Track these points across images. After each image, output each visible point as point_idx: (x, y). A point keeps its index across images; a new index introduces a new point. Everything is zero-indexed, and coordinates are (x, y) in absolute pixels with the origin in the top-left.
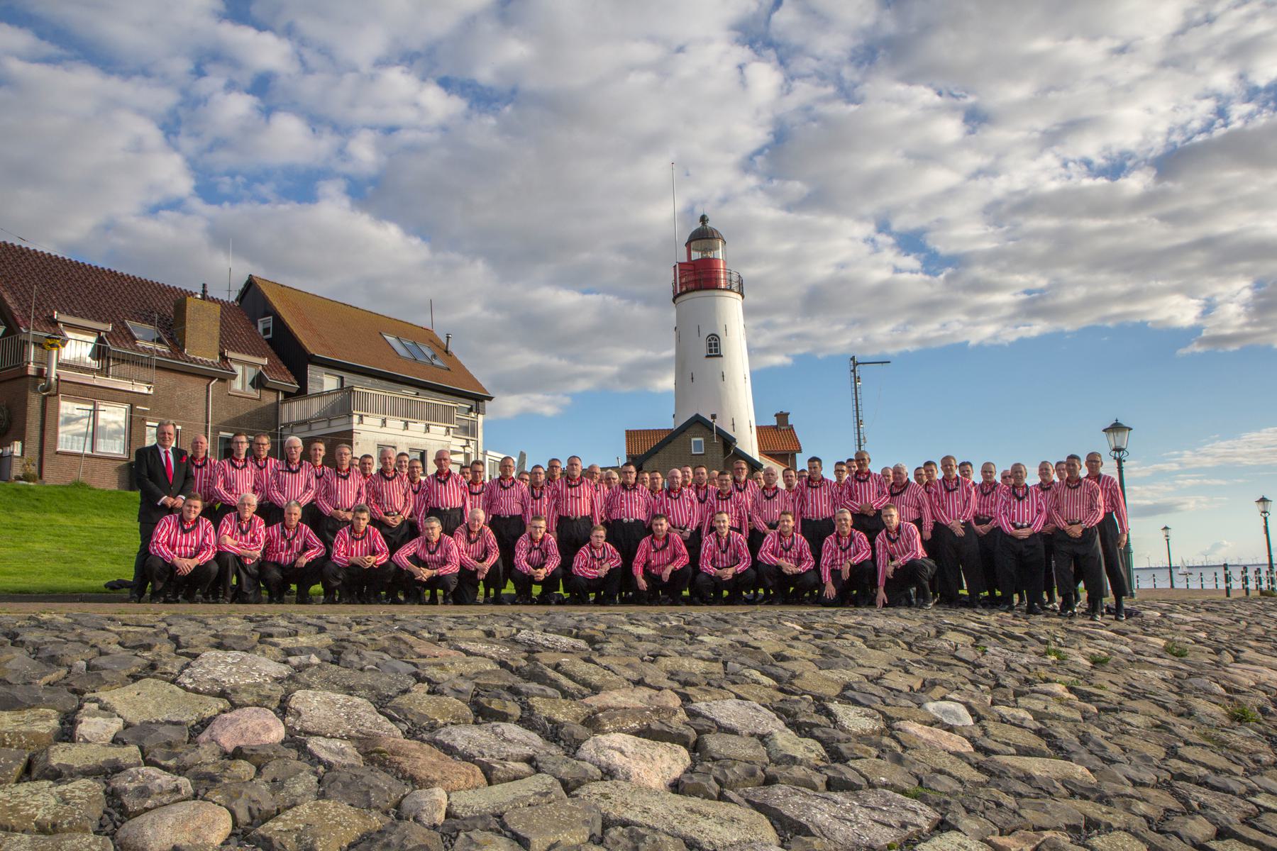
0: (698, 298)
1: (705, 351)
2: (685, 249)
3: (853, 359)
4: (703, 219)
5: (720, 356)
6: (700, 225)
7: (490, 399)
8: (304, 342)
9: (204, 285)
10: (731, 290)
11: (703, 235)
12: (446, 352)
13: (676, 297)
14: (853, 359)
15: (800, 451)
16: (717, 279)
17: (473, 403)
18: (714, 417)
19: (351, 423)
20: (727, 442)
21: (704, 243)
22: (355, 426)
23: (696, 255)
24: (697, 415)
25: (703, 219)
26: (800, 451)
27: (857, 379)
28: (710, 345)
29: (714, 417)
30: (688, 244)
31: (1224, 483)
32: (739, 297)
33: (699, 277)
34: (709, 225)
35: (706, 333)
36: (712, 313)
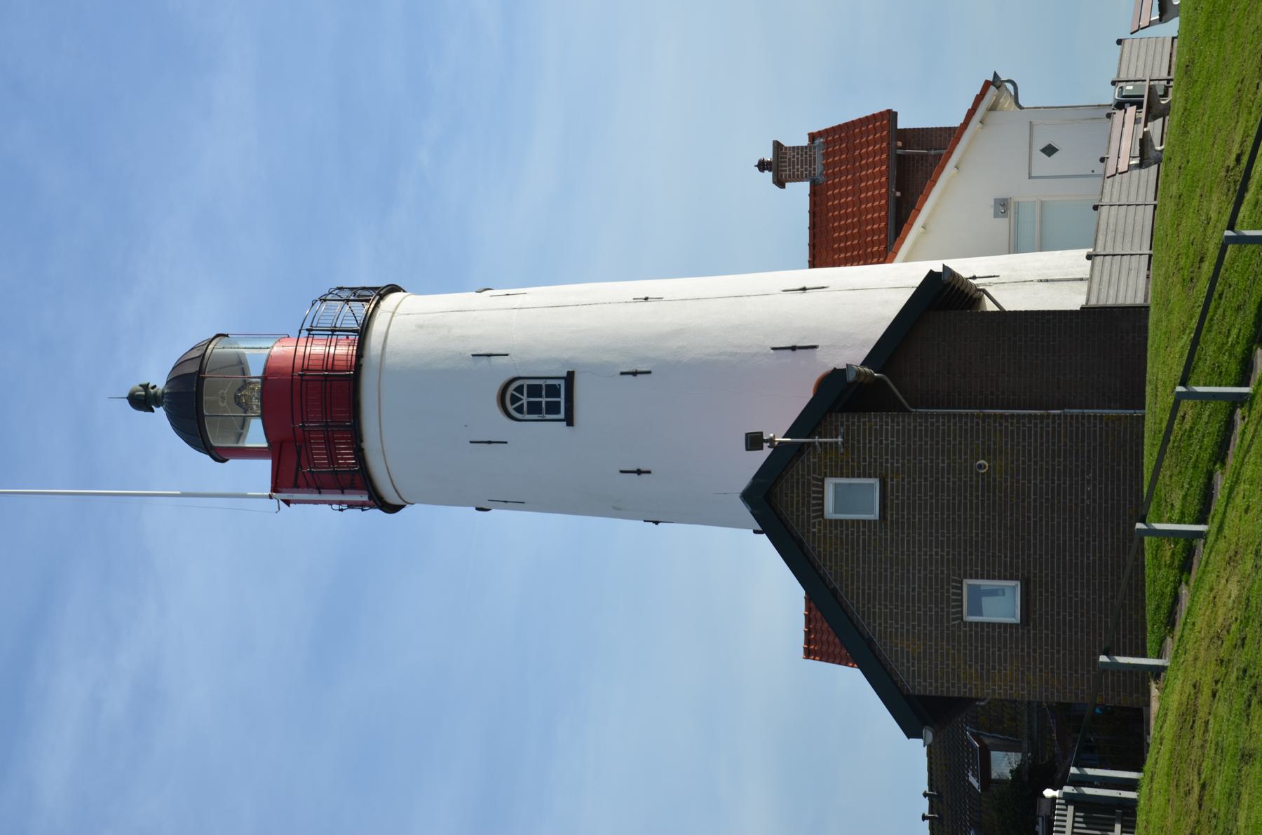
0: (387, 438)
1: (553, 429)
2: (232, 463)
4: (142, 400)
5: (570, 378)
6: (160, 412)
8: (1147, 398)
9: (649, 472)
10: (362, 332)
11: (190, 402)
13: (392, 509)
15: (891, 116)
16: (328, 363)
18: (754, 441)
20: (839, 396)
21: (216, 402)
23: (256, 436)
24: (747, 496)
25: (142, 400)
26: (891, 116)
28: (534, 408)
29: (754, 441)
30: (220, 455)
32: (393, 299)
33: (315, 429)
34: (159, 381)
35: (496, 423)
36: (439, 376)
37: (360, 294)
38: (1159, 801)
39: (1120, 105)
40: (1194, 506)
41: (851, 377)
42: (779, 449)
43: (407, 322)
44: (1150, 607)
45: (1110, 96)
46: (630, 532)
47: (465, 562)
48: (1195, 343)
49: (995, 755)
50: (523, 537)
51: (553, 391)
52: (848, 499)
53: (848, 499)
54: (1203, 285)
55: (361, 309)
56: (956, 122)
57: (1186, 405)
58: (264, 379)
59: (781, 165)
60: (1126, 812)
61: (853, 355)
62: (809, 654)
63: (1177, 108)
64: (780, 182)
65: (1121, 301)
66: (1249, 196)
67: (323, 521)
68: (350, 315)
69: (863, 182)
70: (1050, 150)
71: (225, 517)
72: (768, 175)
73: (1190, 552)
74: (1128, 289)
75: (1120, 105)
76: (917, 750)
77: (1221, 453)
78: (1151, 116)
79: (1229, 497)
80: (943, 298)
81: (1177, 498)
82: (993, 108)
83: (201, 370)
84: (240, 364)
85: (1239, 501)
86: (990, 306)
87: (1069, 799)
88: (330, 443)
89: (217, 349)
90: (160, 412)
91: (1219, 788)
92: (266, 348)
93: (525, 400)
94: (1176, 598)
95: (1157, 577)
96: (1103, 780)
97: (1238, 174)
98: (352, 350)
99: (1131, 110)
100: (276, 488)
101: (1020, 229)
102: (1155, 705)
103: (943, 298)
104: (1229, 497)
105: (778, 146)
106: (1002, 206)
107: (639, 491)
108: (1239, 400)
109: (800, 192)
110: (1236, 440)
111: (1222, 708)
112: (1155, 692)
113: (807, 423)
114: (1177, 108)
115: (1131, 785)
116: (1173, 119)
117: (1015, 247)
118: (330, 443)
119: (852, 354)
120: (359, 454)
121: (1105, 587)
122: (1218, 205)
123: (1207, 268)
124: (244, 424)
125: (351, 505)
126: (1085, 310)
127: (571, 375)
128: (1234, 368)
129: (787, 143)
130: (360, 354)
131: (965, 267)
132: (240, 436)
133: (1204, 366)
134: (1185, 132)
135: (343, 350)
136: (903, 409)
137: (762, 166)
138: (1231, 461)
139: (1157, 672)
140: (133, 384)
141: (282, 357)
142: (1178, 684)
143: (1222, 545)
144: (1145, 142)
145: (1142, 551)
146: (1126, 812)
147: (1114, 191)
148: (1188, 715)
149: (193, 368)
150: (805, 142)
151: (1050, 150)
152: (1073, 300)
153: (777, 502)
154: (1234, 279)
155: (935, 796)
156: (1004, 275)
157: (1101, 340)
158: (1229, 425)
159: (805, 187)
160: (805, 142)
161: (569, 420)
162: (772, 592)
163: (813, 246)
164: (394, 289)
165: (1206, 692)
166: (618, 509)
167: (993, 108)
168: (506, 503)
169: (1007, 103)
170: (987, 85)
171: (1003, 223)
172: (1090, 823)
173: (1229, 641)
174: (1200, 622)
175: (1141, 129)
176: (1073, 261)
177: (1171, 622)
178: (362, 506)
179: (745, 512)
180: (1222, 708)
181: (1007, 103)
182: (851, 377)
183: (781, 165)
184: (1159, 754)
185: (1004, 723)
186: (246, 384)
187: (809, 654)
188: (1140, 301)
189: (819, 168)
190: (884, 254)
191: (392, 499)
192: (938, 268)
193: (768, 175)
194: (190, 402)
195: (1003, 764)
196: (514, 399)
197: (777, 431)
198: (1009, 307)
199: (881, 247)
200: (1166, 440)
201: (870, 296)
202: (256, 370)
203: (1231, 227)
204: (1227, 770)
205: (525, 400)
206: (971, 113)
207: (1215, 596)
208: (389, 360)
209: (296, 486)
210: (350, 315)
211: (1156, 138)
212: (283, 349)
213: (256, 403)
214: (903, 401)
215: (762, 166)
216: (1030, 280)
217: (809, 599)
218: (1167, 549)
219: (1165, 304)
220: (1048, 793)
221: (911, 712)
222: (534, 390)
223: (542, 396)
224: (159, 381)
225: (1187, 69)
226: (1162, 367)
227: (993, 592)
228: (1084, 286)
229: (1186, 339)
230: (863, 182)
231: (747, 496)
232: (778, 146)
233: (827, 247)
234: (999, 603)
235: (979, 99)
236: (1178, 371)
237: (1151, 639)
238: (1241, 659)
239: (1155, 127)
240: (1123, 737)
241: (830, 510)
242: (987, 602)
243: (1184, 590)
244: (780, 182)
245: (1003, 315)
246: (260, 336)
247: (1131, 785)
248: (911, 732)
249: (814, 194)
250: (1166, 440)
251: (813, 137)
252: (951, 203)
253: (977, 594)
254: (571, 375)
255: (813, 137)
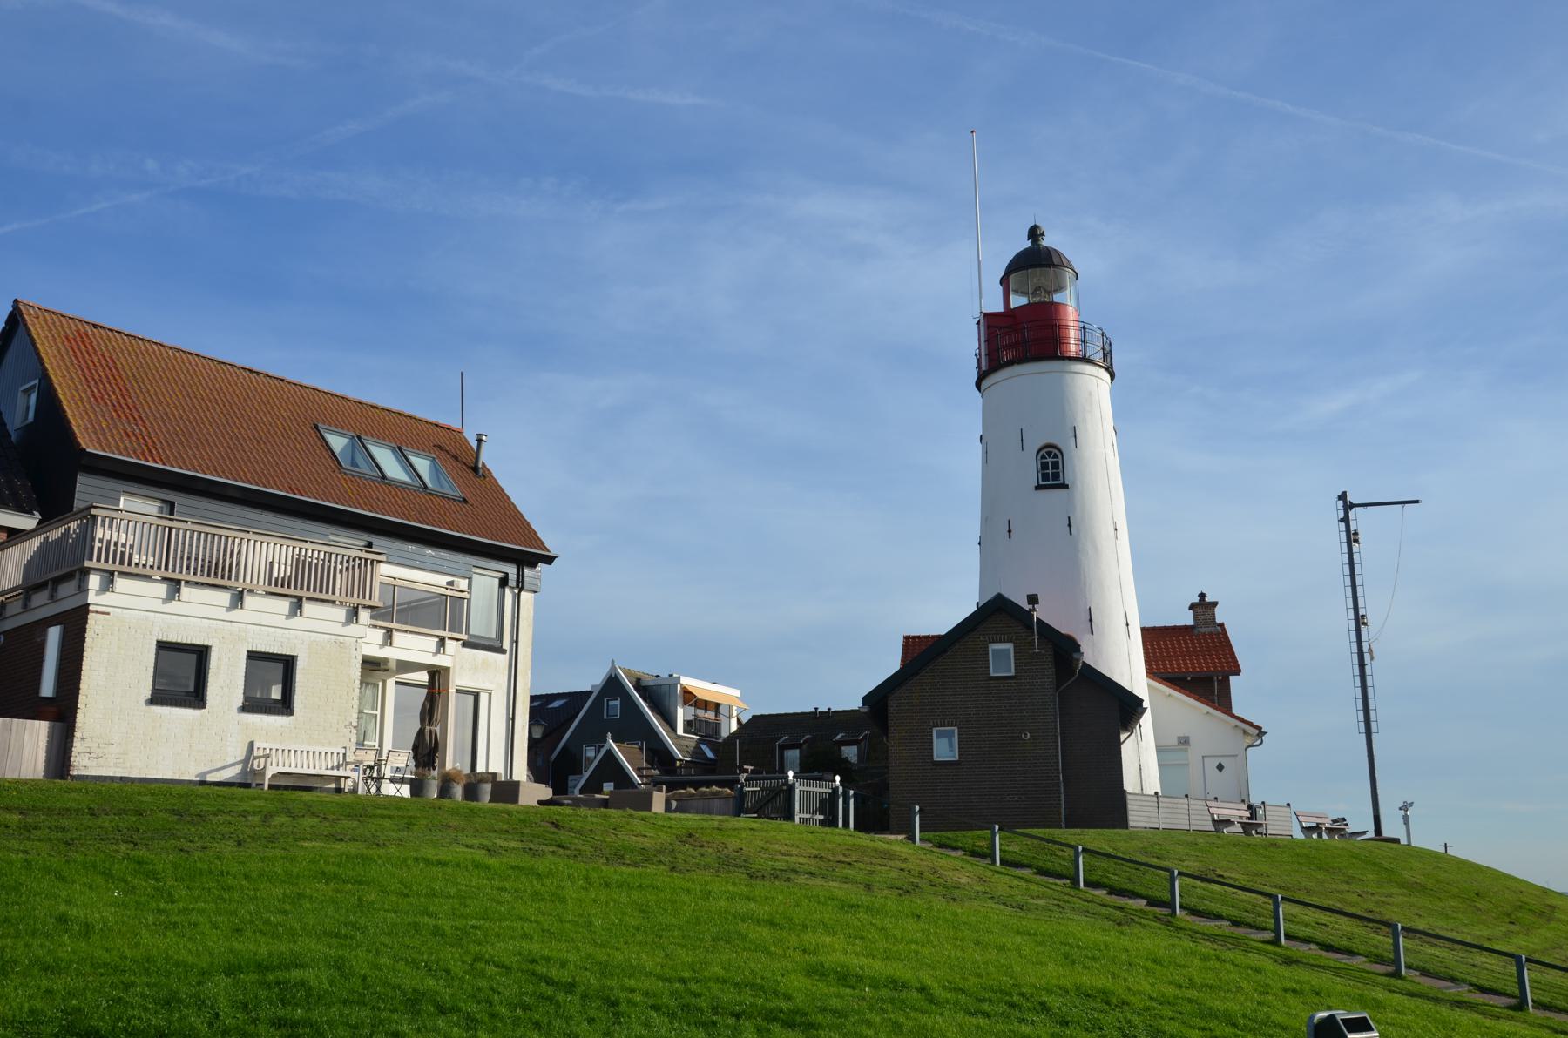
0: (1020, 379)
1: (1032, 478)
3: (1343, 497)
4: (1034, 233)
6: (1028, 244)
7: (549, 560)
10: (1085, 359)
11: (1036, 261)
12: (475, 469)
13: (978, 386)
14: (1343, 497)
15: (1237, 672)
16: (1064, 340)
17: (511, 570)
18: (1033, 599)
19: (83, 589)
20: (1063, 649)
21: (1036, 276)
22: (92, 598)
23: (1017, 301)
24: (999, 597)
25: (1034, 233)
26: (1237, 672)
27: (1352, 538)
28: (1045, 466)
29: (1033, 599)
30: (1004, 281)
31: (554, 756)
32: (1107, 376)
33: (1024, 335)
34: (1046, 242)
35: (1035, 443)
36: (1061, 409)
37: (1108, 355)
38: (839, 839)
39: (1250, 807)
40: (1009, 857)
41: (1075, 656)
42: (1029, 614)
43: (1093, 386)
44: (949, 834)
45: (1255, 801)
46: (972, 528)
47: (950, 433)
48: (1109, 856)
49: (855, 749)
50: (968, 462)
51: (1056, 476)
52: (1001, 657)
53: (1001, 657)
54: (1143, 859)
55: (1098, 357)
56: (1235, 711)
57: (1071, 852)
58: (1052, 303)
59: (1203, 607)
60: (831, 822)
61: (1089, 657)
62: (907, 638)
63: (1249, 840)
64: (1192, 607)
65: (1130, 813)
66: (1198, 883)
67: (968, 344)
68: (1095, 351)
69: (1196, 657)
70: (1220, 767)
71: (975, 286)
72: (1197, 599)
73: (983, 856)
74: (1138, 817)
75: (1250, 807)
76: (855, 703)
77: (1041, 872)
78: (1244, 825)
79: (1017, 877)
80: (1127, 709)
81: (1014, 848)
82: (1245, 732)
83: (1055, 266)
84: (1060, 288)
85: (1016, 882)
86: (1123, 736)
87: (835, 790)
88: (1016, 345)
89: (1069, 274)
90: (1028, 244)
91: (849, 872)
92: (1071, 304)
93: (1049, 460)
94: (955, 849)
95: (968, 838)
96: (847, 808)
97: (1211, 876)
98: (1073, 354)
99: (1247, 814)
100: (986, 315)
101: (1171, 752)
102: (892, 837)
103: (1127, 709)
104: (1017, 877)
105: (1215, 604)
106: (1184, 741)
107: (998, 532)
108: (1075, 881)
109: (1187, 619)
110: (1051, 880)
111: (894, 874)
112: (900, 837)
113: (1046, 630)
114: (1249, 840)
115: (846, 824)
116: (1243, 838)
117: (1159, 749)
118: (1016, 345)
119: (1090, 656)
120: (1011, 363)
121: (957, 809)
122: (1192, 865)
123: (1154, 861)
124: (1024, 293)
125: (979, 361)
126: (1123, 794)
127: (1066, 487)
128: (1094, 878)
129: (1217, 610)
130: (1070, 359)
131: (1146, 721)
132: (1016, 292)
133: (1094, 861)
134: (1235, 845)
135: (1073, 348)
136: (1058, 687)
137: (1202, 596)
138: (1038, 878)
139: (912, 838)
140: (1044, 227)
141: (1066, 313)
142: (906, 850)
143: (989, 874)
144: (1228, 823)
145: (981, 828)
146: (831, 822)
147: (1197, 806)
148: (888, 856)
149: (1056, 261)
150: (1218, 620)
151: (1220, 767)
152: (1130, 785)
153: (997, 615)
154: (1148, 876)
155: (829, 715)
156: (1143, 744)
157: (1107, 803)
158: (1060, 876)
159: (1191, 622)
160: (1218, 620)
161: (1038, 487)
162: (946, 608)
163: (1154, 629)
164: (1112, 377)
165: (903, 866)
166: (985, 520)
167: (1245, 732)
168: (986, 453)
169: (1248, 741)
170: (1259, 728)
171: (1175, 742)
172: (823, 802)
173: (933, 878)
174: (942, 862)
175: (1236, 820)
176: (1153, 784)
177: (941, 846)
178: (979, 367)
179: (989, 596)
180: (894, 874)
181: (1248, 741)
182: (1075, 656)
183: (1203, 607)
184: (864, 839)
185: (875, 751)
186: (1048, 293)
187: (907, 638)
188: (1131, 824)
189: (1203, 630)
190: (1151, 672)
191: (985, 384)
192: (1145, 704)
193: (1197, 599)
194: (1036, 261)
195: (851, 753)
196: (1049, 453)
197: (1039, 613)
198: (1123, 747)
199: (1155, 669)
200: (1048, 841)
201: (1126, 665)
202: (1057, 298)
203: (1180, 873)
204: (860, 877)
205: (1049, 460)
206: (1241, 720)
207: (957, 869)
208: (1068, 377)
209: (988, 327)
210: (1095, 351)
211: (1231, 829)
212: (1071, 313)
213: (1037, 299)
214: (1110, 451)
215: (1202, 596)
216: (1140, 760)
217: (939, 637)
218: (984, 844)
219: (1131, 838)
220: (838, 778)
221: (878, 699)
222: (1055, 465)
223: (1052, 470)
224: (1046, 242)
225: (1274, 844)
226: (1092, 837)
227: (951, 745)
228: (1138, 791)
229: (1110, 851)
230: (1196, 657)
231: (999, 597)
232: (1215, 604)
233: (1151, 636)
234: (945, 748)
235: (1250, 724)
236: (1091, 847)
237: (931, 835)
238: (924, 884)
239: (1238, 828)
240: (873, 819)
241: (994, 646)
242: (945, 741)
243: (960, 853)
244: (1192, 607)
245: (1119, 744)
246: (1078, 298)
247: (846, 824)
248: (865, 699)
249: (1186, 627)
250: (1048, 841)
251: (1222, 625)
252: (1186, 711)
253: (950, 735)
254: (1066, 487)
255: (1222, 625)
